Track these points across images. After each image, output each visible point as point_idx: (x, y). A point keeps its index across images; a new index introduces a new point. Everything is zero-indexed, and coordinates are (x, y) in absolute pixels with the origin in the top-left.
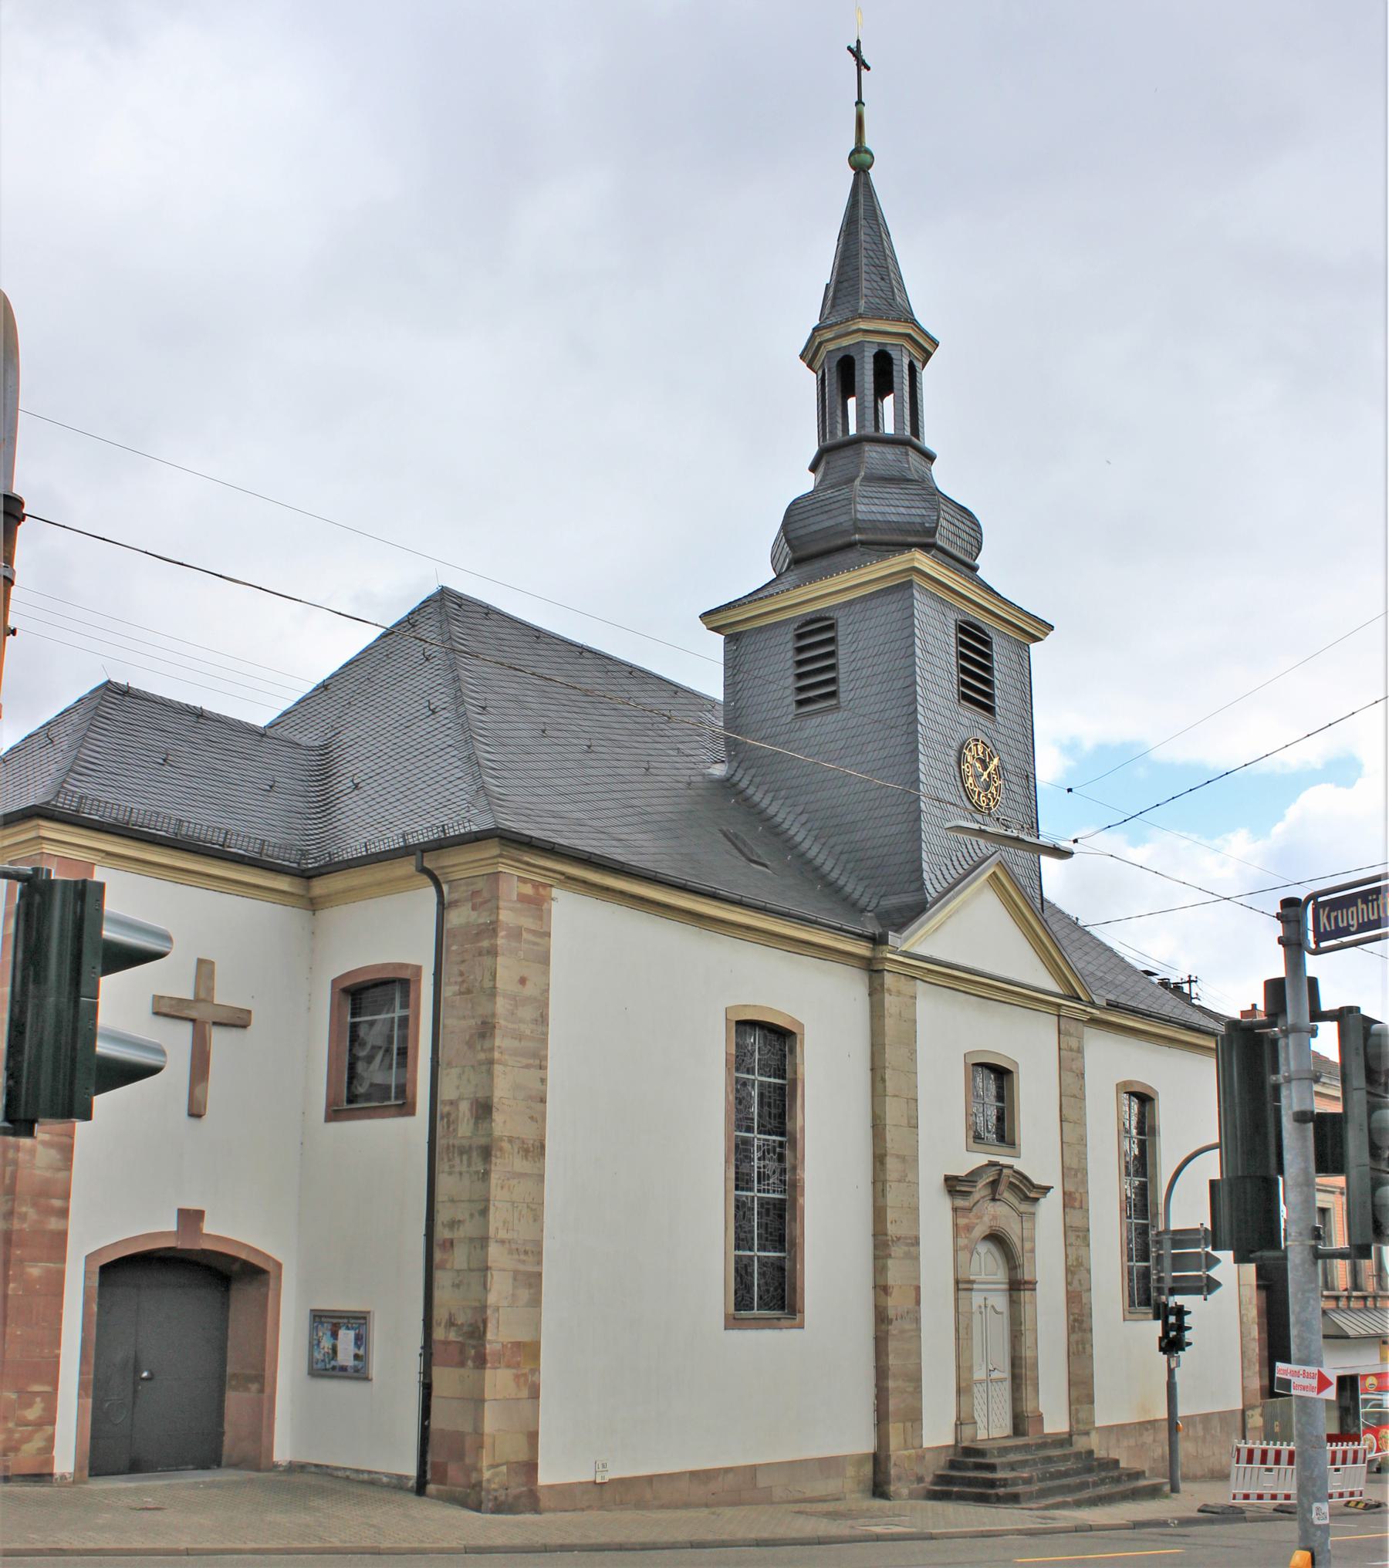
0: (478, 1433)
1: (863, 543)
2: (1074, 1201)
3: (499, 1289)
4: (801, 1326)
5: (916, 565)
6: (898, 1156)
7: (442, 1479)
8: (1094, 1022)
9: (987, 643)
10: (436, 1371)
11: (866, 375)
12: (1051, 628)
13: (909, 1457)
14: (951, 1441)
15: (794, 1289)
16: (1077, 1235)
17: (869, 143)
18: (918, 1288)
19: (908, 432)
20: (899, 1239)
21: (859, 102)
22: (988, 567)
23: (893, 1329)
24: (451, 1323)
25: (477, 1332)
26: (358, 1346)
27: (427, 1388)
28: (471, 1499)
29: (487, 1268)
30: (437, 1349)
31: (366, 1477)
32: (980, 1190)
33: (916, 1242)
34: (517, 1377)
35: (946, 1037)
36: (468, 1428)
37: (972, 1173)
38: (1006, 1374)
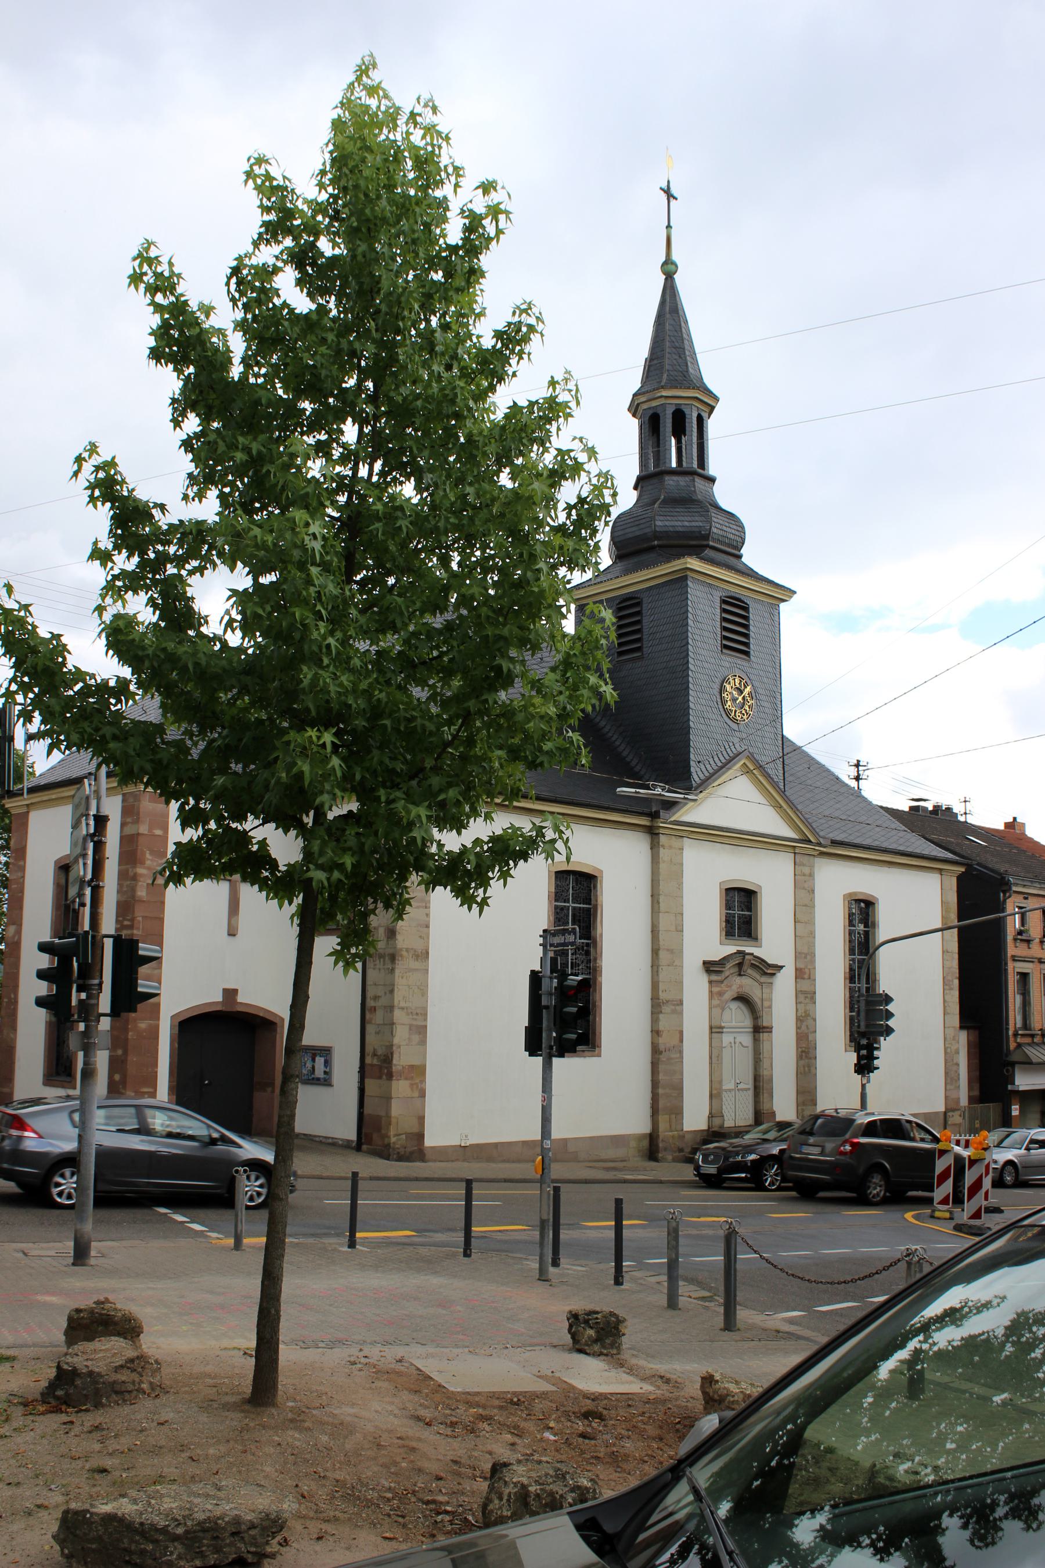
0: (388, 1116)
1: (659, 546)
2: (804, 973)
3: (401, 1034)
4: (599, 1055)
5: (689, 566)
6: (668, 950)
7: (369, 1142)
8: (822, 854)
9: (746, 609)
10: (367, 1081)
11: (667, 424)
12: (794, 592)
13: (673, 1137)
14: (705, 1127)
15: (594, 1033)
16: (806, 996)
17: (675, 257)
18: (681, 1033)
19: (695, 465)
20: (667, 1002)
21: (669, 227)
22: (751, 556)
23: (663, 1058)
24: (375, 1055)
25: (387, 1059)
26: (326, 1066)
27: (362, 1090)
28: (385, 1152)
29: (393, 1024)
30: (367, 1069)
31: (330, 1141)
32: (729, 969)
33: (681, 1003)
34: (412, 1085)
35: (704, 875)
36: (383, 1113)
37: (724, 958)
38: (750, 1085)
